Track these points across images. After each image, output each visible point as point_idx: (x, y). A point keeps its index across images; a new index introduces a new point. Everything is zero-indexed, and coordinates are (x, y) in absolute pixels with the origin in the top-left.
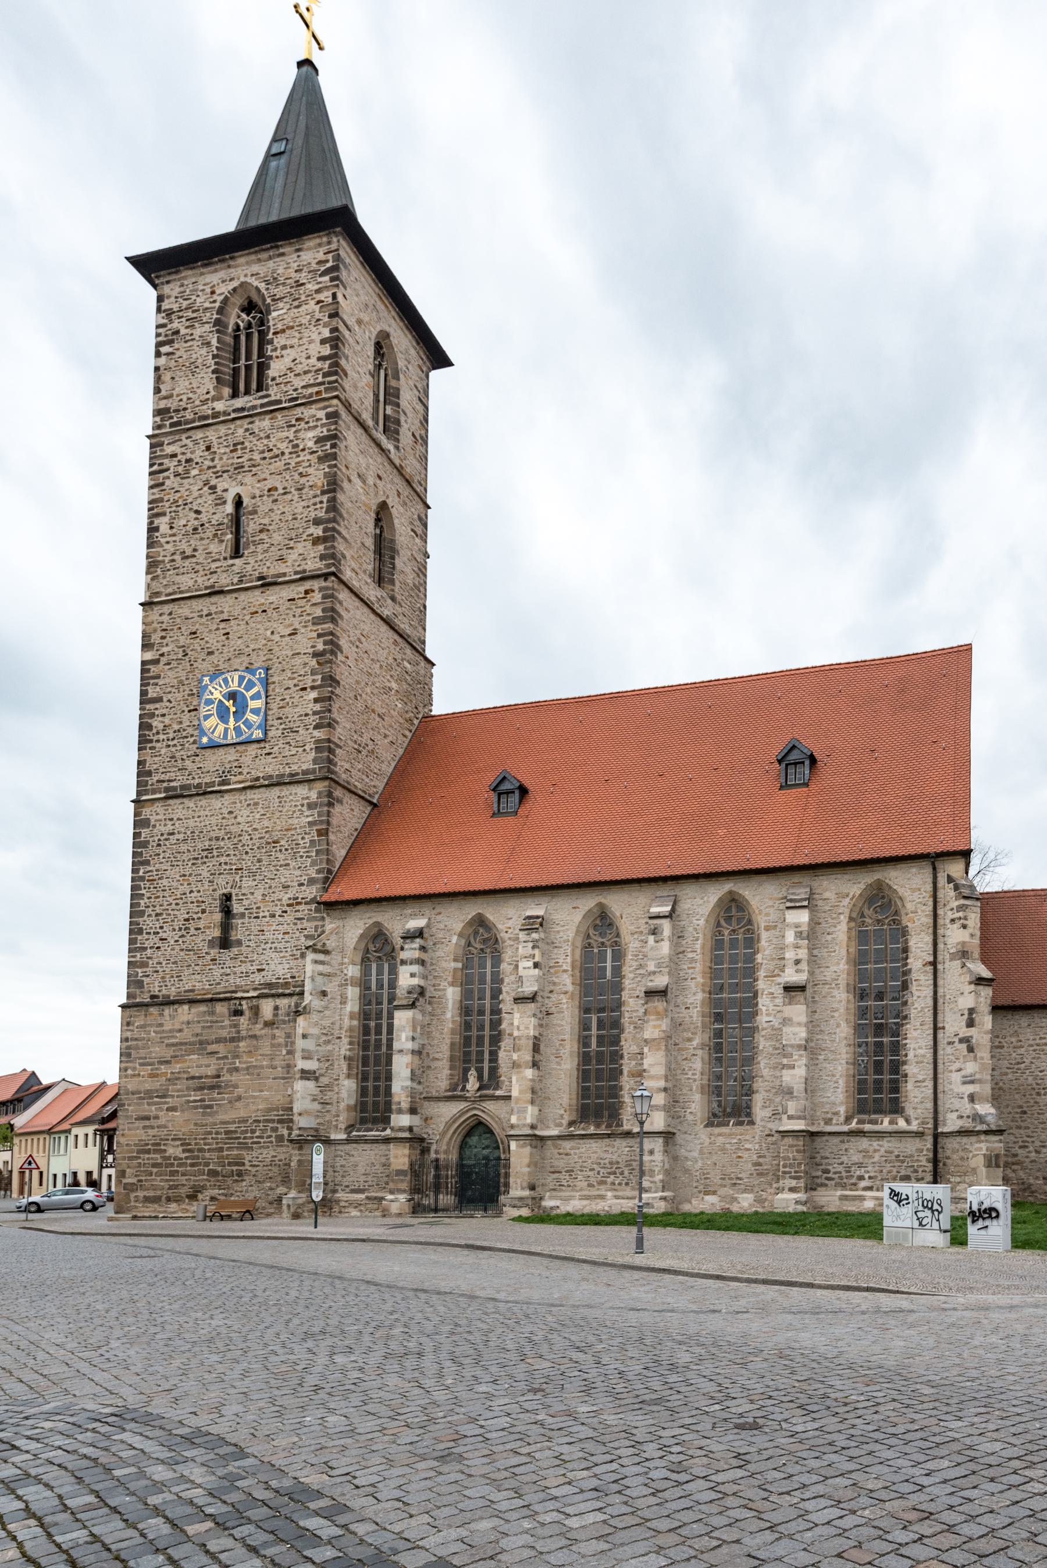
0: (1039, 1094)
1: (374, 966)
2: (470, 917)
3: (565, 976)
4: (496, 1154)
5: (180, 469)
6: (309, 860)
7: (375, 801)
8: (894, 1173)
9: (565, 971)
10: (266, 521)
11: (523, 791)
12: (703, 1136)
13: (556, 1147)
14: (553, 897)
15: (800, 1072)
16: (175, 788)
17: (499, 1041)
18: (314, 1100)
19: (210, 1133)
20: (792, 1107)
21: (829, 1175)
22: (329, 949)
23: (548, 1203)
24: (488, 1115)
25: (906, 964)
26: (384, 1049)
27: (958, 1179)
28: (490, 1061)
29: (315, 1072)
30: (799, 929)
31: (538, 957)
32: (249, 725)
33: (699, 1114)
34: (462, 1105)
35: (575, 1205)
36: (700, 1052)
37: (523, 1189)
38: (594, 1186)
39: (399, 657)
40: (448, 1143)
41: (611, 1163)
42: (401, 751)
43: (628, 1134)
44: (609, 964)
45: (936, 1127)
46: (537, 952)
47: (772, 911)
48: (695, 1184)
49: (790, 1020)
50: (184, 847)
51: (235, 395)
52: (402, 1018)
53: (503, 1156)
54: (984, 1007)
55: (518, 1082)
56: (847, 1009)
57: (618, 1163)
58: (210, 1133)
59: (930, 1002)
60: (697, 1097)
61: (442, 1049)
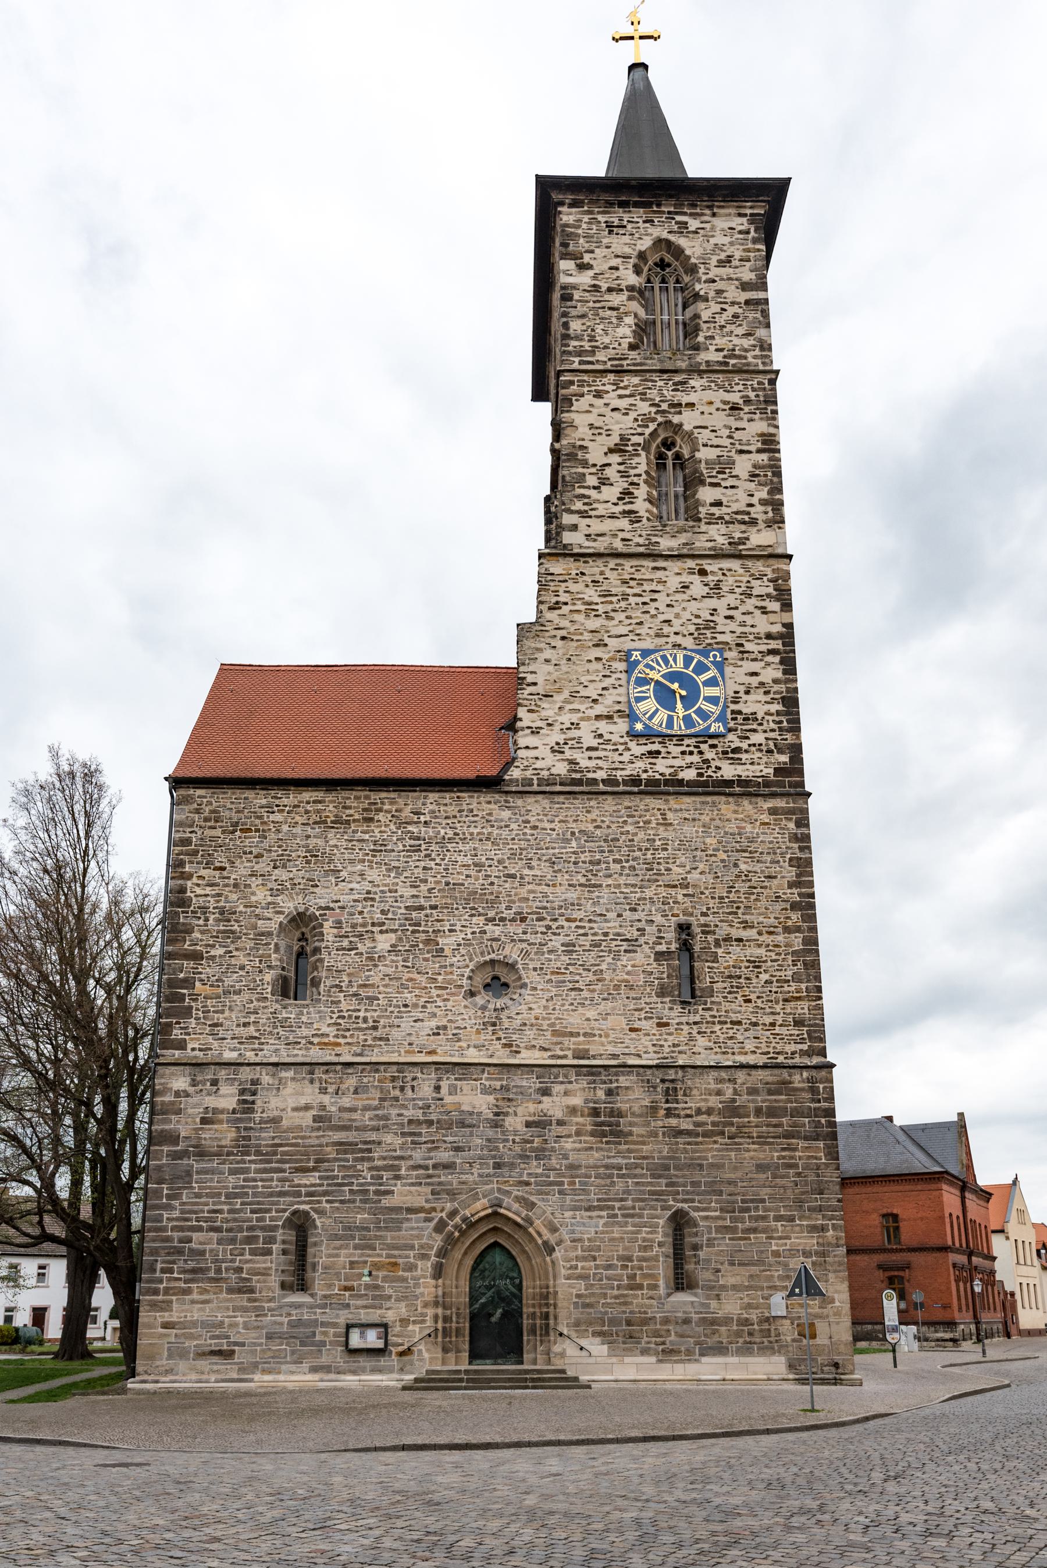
32: (703, 715)
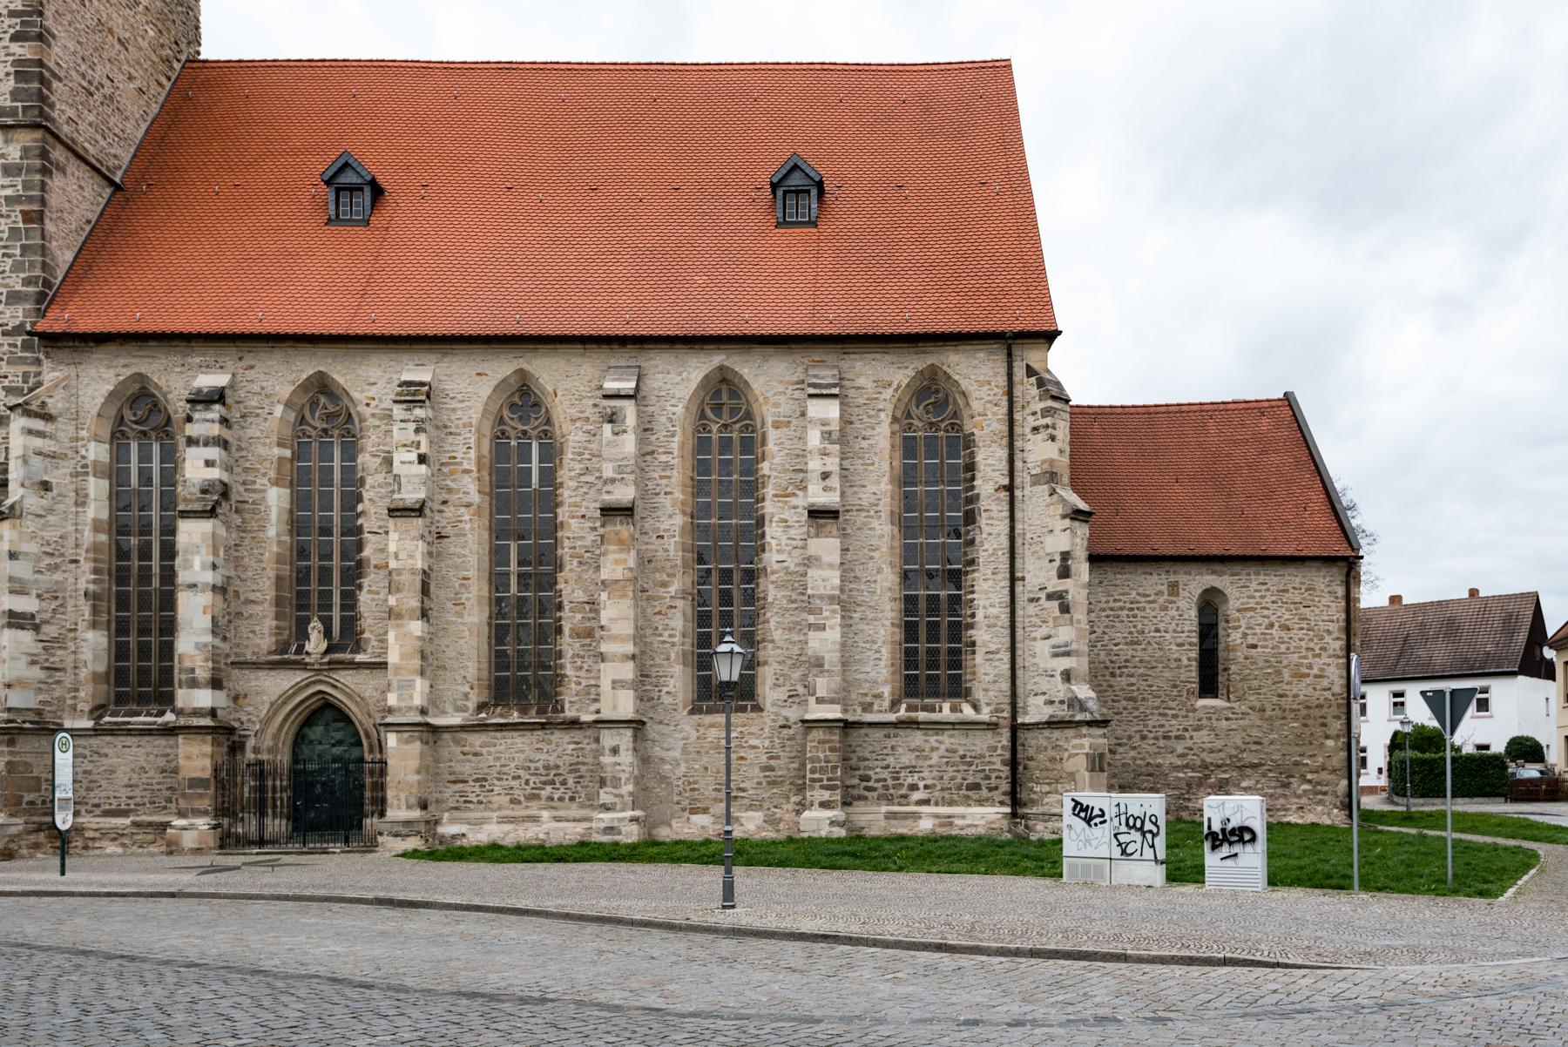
0: (1113, 675)
1: (134, 446)
2: (305, 376)
3: (467, 479)
4: (355, 753)
6: (10, 261)
7: (117, 180)
8: (959, 780)
9: (467, 472)
11: (377, 191)
12: (687, 728)
13: (457, 742)
14: (444, 355)
15: (833, 634)
17: (360, 576)
18: (34, 663)
20: (823, 686)
21: (870, 784)
22: (53, 412)
23: (447, 829)
24: (342, 691)
25: (973, 488)
26: (156, 582)
27: (1046, 788)
28: (343, 608)
29: (33, 616)
30: (827, 428)
31: (419, 444)
33: (680, 696)
34: (299, 676)
35: (480, 836)
36: (680, 603)
37: (409, 807)
38: (519, 802)
40: (276, 737)
41: (547, 768)
42: (155, 108)
43: (574, 724)
44: (535, 465)
46: (423, 438)
47: (783, 399)
48: (676, 799)
49: (818, 559)
52: (191, 533)
53: (368, 757)
54: (1081, 554)
55: (398, 643)
56: (892, 547)
57: (557, 767)
59: (1005, 543)
60: (678, 669)
61: (262, 586)
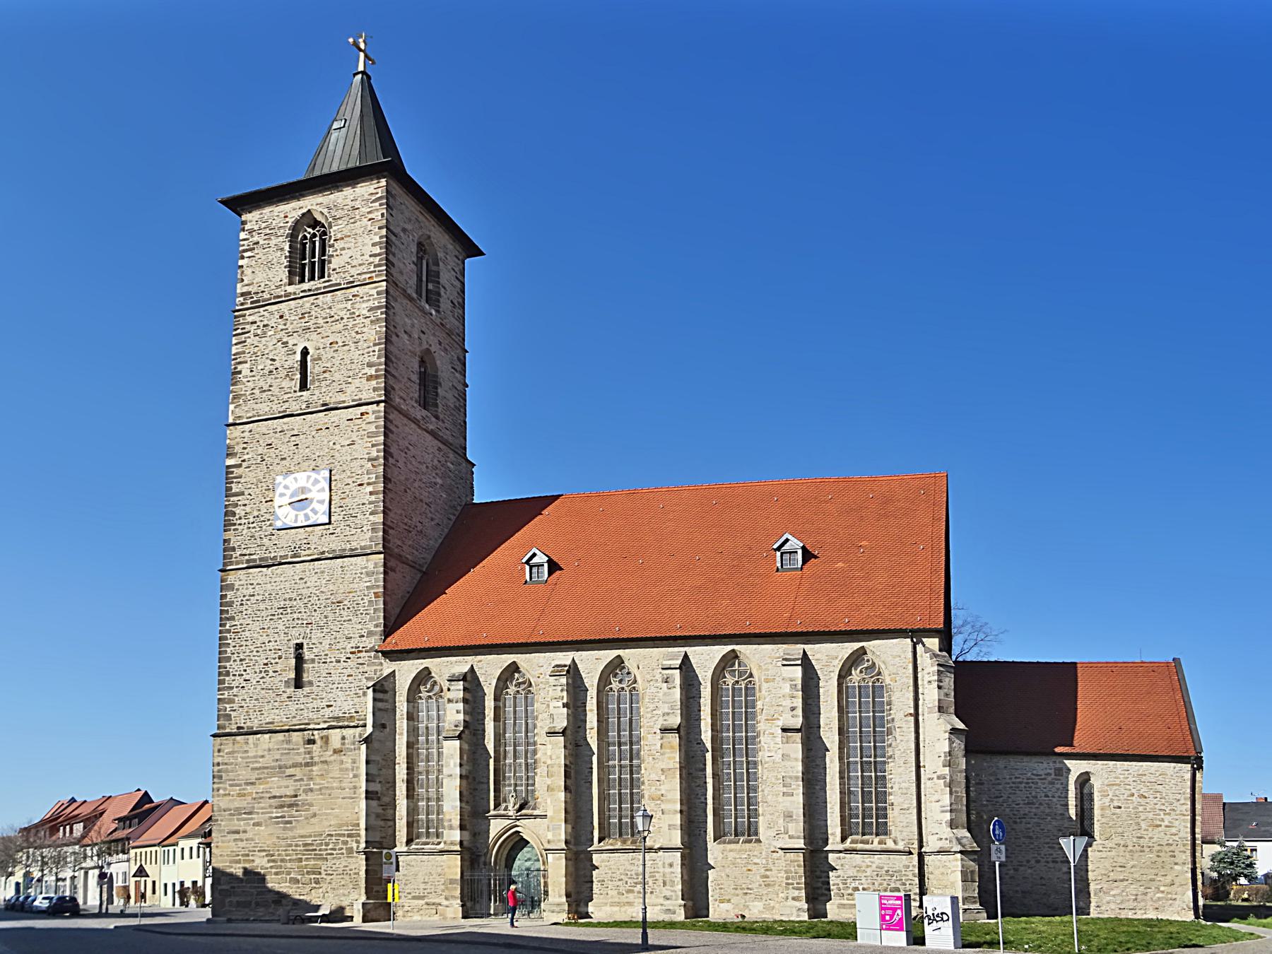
5: (259, 332)
10: (329, 365)
16: (255, 560)
19: (291, 845)
32: (315, 512)
39: (442, 459)
45: (921, 846)
50: (262, 606)
51: (302, 281)
58: (291, 845)
